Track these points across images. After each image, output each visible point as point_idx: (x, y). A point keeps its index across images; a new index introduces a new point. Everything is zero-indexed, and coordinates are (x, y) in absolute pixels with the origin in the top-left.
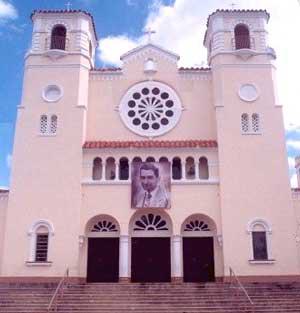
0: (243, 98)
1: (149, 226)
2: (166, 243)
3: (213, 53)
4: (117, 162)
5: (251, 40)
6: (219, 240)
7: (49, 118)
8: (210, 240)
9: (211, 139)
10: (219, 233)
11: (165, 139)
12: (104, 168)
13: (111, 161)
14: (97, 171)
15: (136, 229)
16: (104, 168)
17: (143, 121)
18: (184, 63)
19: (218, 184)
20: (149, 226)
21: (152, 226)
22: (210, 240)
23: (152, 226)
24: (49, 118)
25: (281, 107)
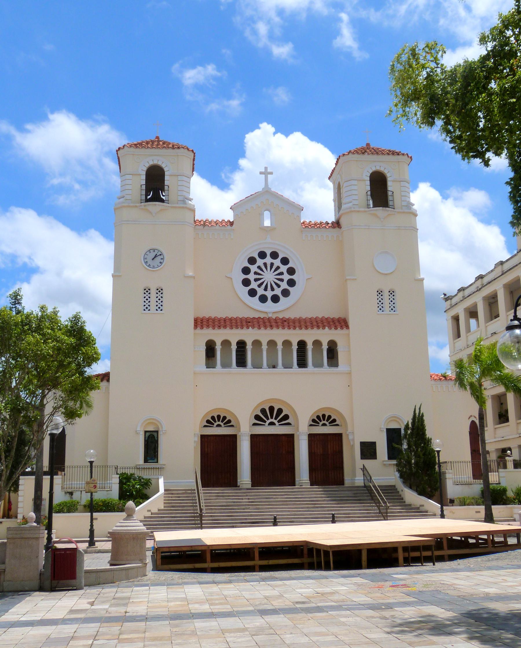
0: (379, 270)
1: (271, 420)
2: (290, 439)
3: (341, 212)
4: (325, 347)
5: (390, 193)
6: (351, 437)
7: (153, 292)
8: (339, 436)
9: (342, 316)
10: (350, 430)
11: (287, 315)
12: (315, 561)
13: (287, 344)
14: (241, 168)
15: (254, 424)
16: (315, 561)
17: (260, 291)
18: (307, 217)
19: (350, 373)
20: (271, 420)
21: (273, 420)
22: (339, 436)
23: (273, 420)
24: (153, 292)
25: (422, 280)
